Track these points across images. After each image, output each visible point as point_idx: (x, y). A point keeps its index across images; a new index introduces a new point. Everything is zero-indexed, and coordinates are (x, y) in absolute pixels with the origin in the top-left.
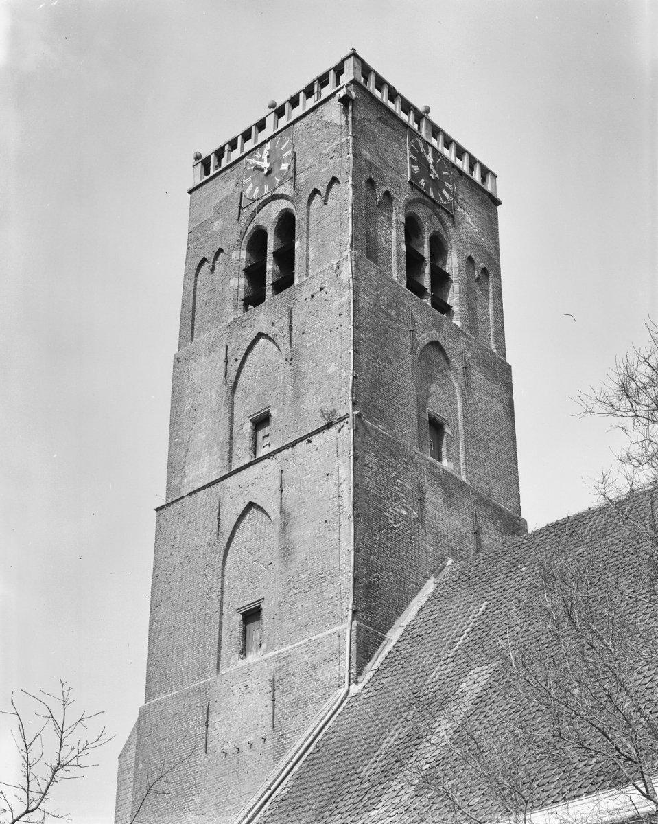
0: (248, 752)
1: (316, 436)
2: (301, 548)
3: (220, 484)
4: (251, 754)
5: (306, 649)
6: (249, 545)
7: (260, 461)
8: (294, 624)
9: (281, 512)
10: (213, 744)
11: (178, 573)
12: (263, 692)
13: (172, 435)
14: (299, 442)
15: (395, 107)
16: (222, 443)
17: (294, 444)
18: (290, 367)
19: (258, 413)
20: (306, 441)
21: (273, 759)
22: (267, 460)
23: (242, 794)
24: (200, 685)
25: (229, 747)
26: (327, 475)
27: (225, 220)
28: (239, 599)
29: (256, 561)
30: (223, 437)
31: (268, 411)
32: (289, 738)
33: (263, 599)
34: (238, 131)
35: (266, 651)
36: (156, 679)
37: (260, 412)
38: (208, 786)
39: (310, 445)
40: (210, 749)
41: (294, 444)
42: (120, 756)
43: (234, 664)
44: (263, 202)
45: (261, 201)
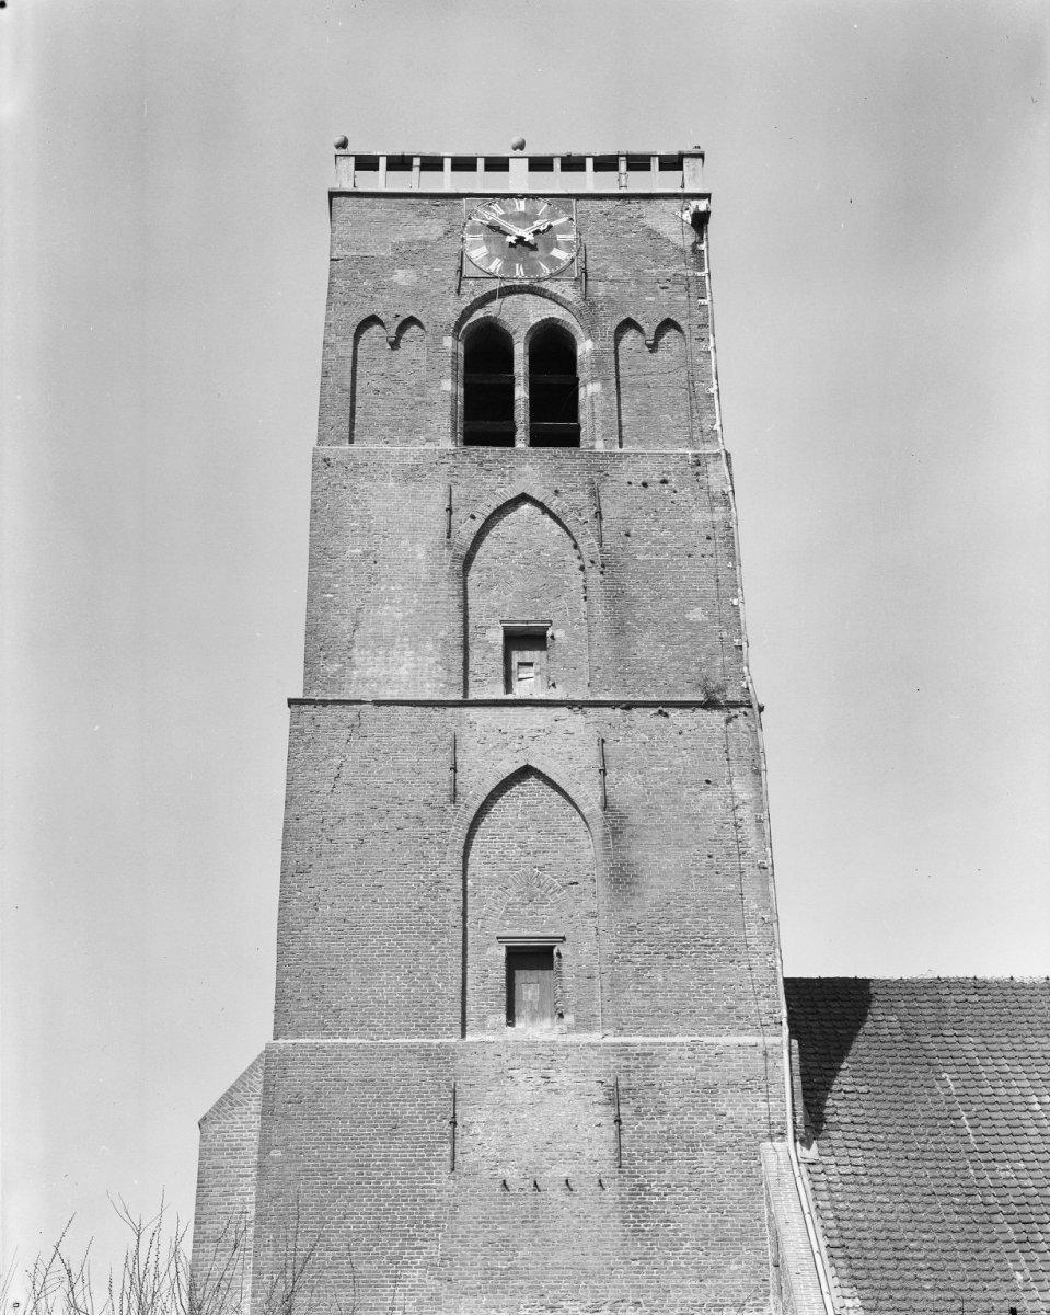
0: (558, 1194)
1: (678, 711)
2: (653, 881)
3: (450, 710)
4: (567, 1199)
5: (691, 1054)
6: (522, 835)
7: (550, 706)
8: (647, 1004)
9: (605, 808)
10: (472, 1157)
11: (348, 830)
12: (589, 1100)
13: (314, 586)
14: (640, 706)
15: (447, 181)
16: (445, 642)
17: (629, 706)
18: (601, 577)
19: (523, 622)
20: (656, 710)
21: (623, 1222)
22: (565, 709)
23: (549, 1265)
24: (430, 1045)
25: (511, 1174)
26: (708, 782)
27: (419, 275)
28: (501, 921)
29: (540, 869)
30: (449, 628)
31: (547, 628)
32: (658, 1195)
33: (564, 938)
34: (448, 150)
35: (570, 1030)
36: (300, 993)
37: (527, 622)
38: (460, 1230)
39: (661, 719)
40: (467, 1159)
41: (629, 706)
42: (204, 1119)
43: (489, 1032)
44: (506, 287)
45: (508, 284)
